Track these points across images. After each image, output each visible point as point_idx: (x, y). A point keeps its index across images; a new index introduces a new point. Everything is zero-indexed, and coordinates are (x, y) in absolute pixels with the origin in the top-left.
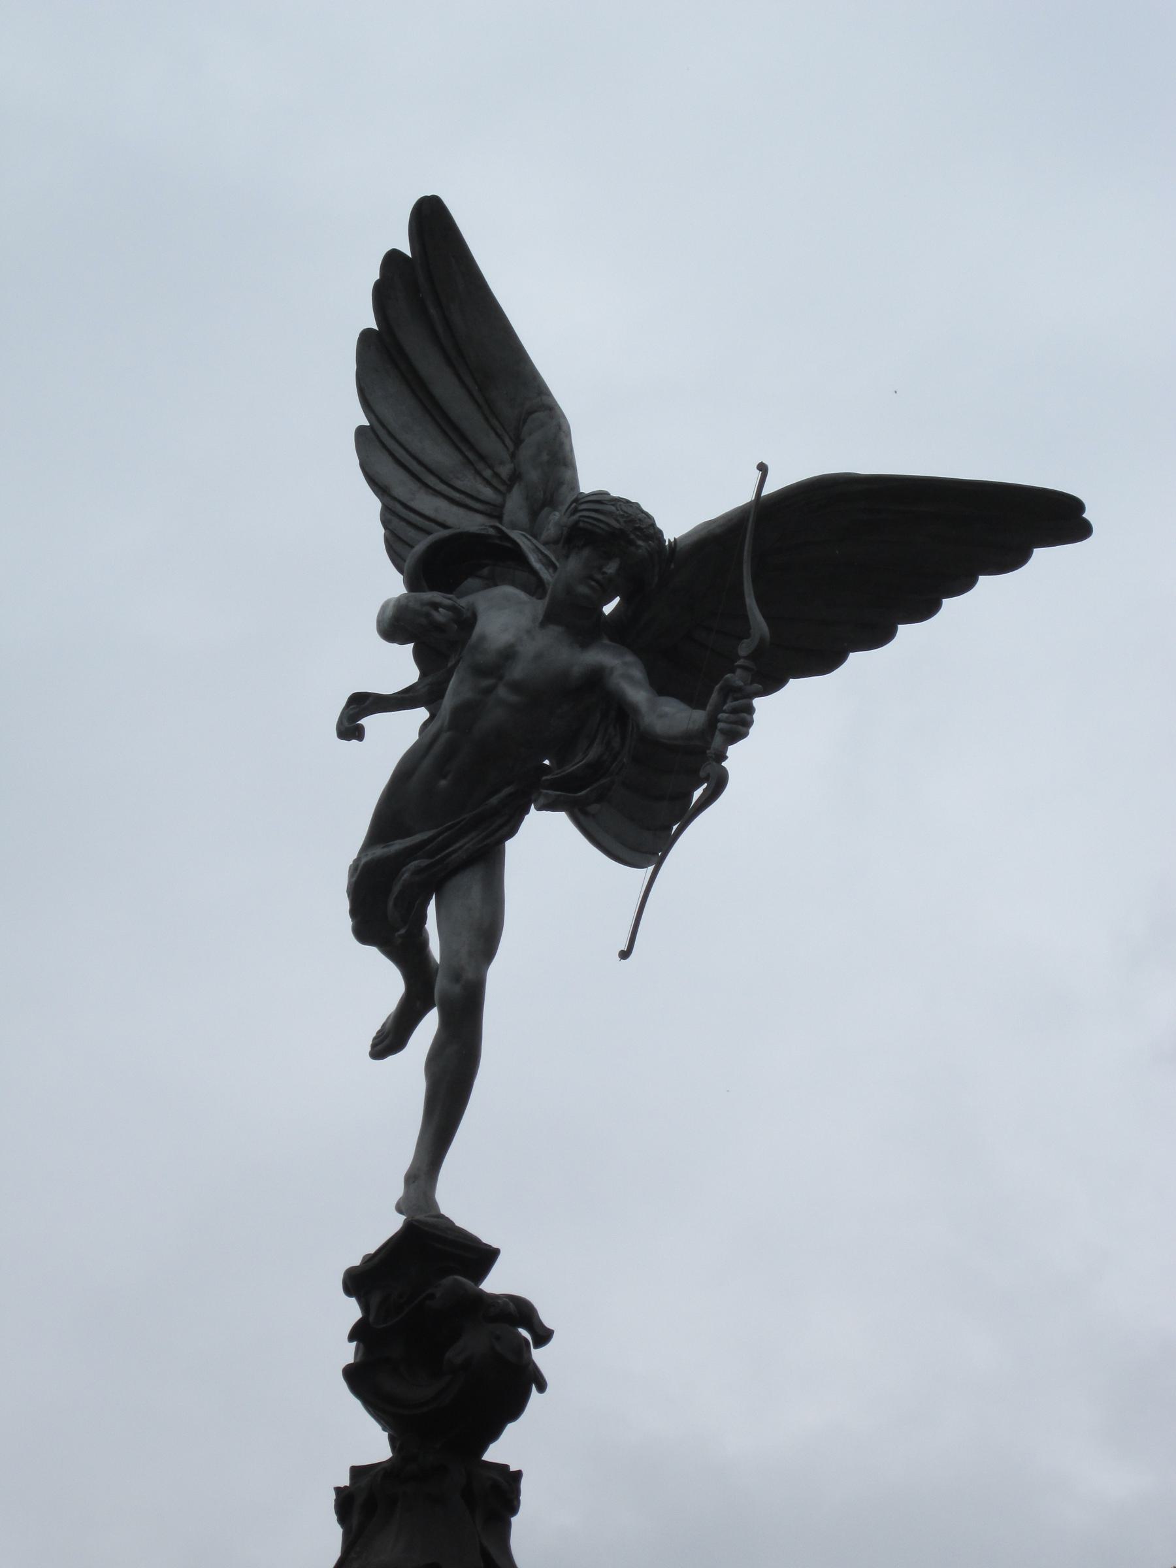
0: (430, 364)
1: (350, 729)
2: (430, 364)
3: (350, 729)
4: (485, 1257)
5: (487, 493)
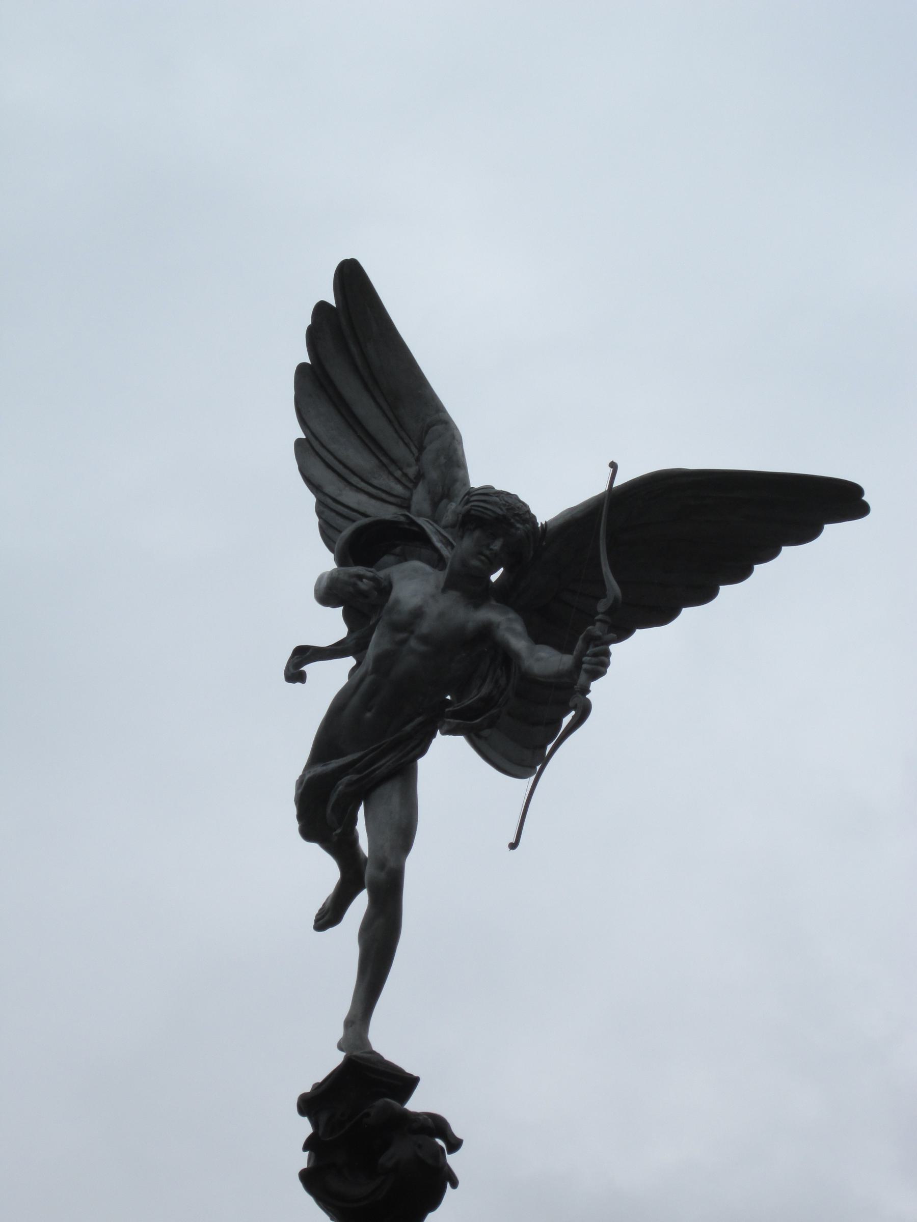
0: (352, 389)
1: (295, 674)
2: (352, 389)
3: (295, 674)
4: (407, 1083)
5: (398, 489)
